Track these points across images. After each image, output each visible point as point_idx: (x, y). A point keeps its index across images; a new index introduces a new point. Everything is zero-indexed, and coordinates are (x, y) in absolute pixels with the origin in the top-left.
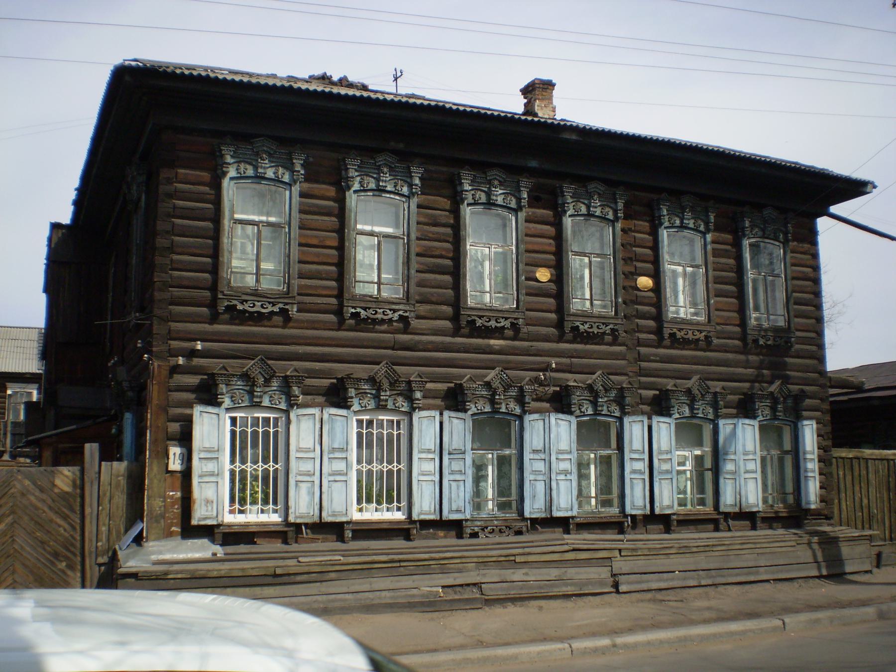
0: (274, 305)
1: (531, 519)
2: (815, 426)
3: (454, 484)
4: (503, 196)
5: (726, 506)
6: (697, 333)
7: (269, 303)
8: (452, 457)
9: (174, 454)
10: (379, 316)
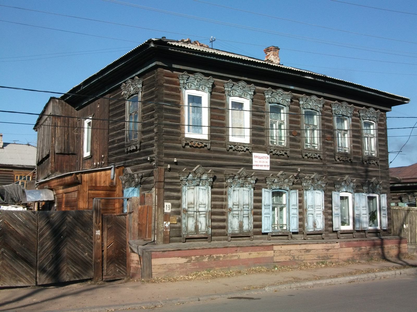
0: (202, 143)
1: (292, 232)
2: (386, 196)
3: (266, 218)
4: (281, 101)
5: (357, 228)
6: (346, 158)
7: (201, 142)
8: (265, 207)
9: (166, 205)
10: (239, 149)
